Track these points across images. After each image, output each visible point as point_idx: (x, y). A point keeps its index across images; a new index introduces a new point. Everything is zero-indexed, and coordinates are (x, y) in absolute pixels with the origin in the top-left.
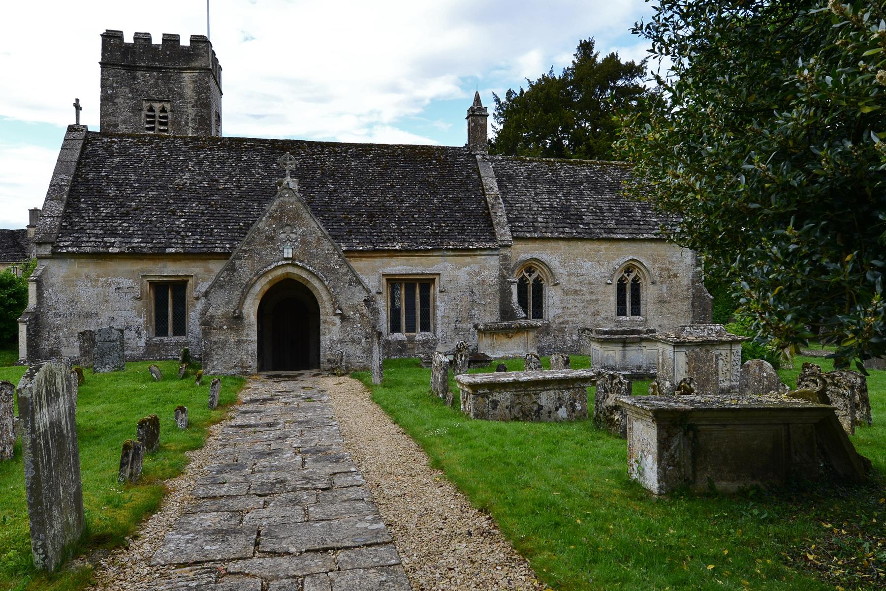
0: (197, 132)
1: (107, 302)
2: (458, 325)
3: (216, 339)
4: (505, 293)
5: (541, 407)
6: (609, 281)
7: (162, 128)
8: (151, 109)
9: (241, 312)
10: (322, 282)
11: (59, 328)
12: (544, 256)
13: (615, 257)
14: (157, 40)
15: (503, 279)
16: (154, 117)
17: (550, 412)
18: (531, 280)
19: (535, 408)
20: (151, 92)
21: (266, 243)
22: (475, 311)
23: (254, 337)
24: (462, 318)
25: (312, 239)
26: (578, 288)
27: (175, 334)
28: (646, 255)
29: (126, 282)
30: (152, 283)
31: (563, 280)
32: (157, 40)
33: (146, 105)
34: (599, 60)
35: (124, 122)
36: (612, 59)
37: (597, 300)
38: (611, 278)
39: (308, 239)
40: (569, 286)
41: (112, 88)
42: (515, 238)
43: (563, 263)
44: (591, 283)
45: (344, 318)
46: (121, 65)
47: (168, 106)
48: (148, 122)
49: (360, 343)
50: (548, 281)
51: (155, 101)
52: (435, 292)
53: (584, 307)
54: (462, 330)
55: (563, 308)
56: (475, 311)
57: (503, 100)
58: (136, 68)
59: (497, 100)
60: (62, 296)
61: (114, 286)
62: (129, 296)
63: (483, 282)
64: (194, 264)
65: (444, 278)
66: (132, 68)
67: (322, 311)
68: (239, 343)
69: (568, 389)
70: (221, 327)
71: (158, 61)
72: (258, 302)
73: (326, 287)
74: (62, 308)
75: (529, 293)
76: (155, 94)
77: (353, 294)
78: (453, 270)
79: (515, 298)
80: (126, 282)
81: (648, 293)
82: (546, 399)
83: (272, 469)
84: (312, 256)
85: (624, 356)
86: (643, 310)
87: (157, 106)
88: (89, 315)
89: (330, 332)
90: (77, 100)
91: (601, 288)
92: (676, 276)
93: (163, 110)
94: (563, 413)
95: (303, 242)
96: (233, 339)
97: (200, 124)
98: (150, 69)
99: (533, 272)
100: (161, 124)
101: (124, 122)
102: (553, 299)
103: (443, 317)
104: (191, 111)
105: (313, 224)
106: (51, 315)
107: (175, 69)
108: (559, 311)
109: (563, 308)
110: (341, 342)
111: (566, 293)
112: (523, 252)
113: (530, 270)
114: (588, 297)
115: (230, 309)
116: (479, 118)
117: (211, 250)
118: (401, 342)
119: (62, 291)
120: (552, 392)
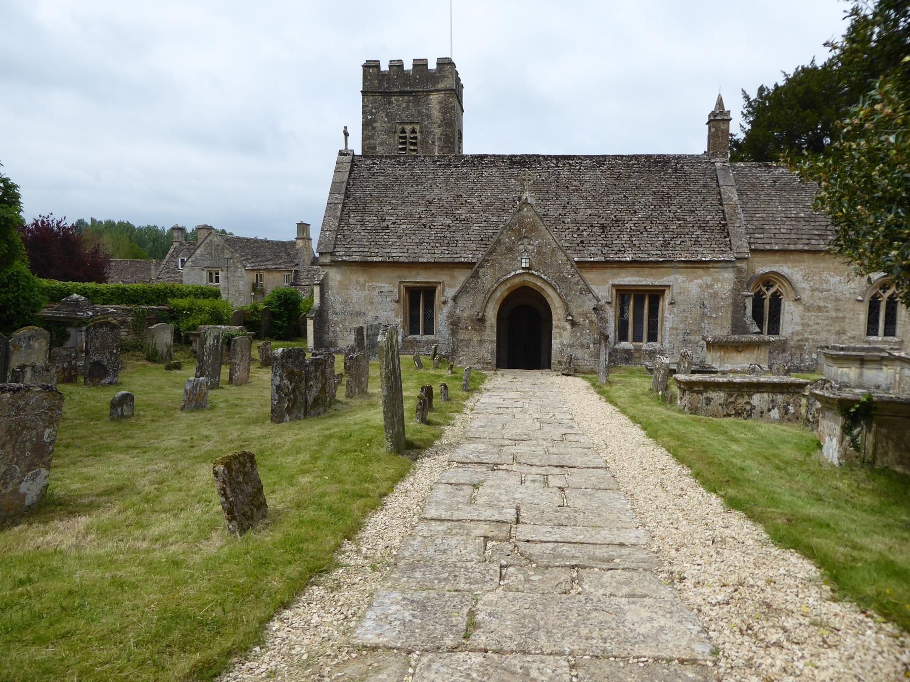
0: (442, 150)
1: (372, 303)
2: (686, 337)
3: (462, 338)
4: (738, 307)
5: (753, 408)
6: (860, 298)
7: (412, 148)
8: (403, 131)
9: (483, 315)
10: (555, 290)
11: (336, 324)
12: (784, 269)
14: (408, 66)
15: (736, 292)
16: (405, 138)
17: (762, 413)
18: (769, 294)
19: (748, 407)
20: (403, 116)
21: (505, 254)
22: (705, 324)
24: (691, 330)
25: (547, 250)
26: (821, 304)
27: (425, 333)
29: (387, 287)
30: (407, 288)
31: (805, 296)
32: (408, 66)
33: (399, 127)
35: (381, 144)
37: (844, 318)
39: (544, 250)
40: (811, 302)
41: (372, 114)
42: (752, 251)
43: (806, 277)
44: (837, 300)
45: (573, 324)
46: (379, 92)
47: (417, 128)
48: (401, 143)
49: (588, 347)
50: (787, 296)
51: (407, 123)
52: (664, 304)
53: (827, 325)
54: (690, 342)
55: (803, 325)
56: (705, 324)
57: (753, 95)
59: (747, 97)
60: (338, 298)
61: (378, 290)
62: (389, 299)
63: (715, 295)
64: (442, 272)
65: (676, 290)
66: (387, 94)
67: (554, 317)
68: (481, 342)
69: (782, 393)
70: (466, 328)
71: (410, 85)
72: (498, 307)
73: (559, 295)
74: (338, 307)
75: (763, 307)
76: (406, 117)
77: (584, 302)
78: (683, 282)
82: (758, 400)
84: (546, 265)
85: (861, 375)
86: (899, 330)
87: (408, 128)
88: (359, 314)
89: (561, 336)
90: (346, 128)
91: (849, 306)
93: (413, 131)
94: (775, 414)
95: (539, 253)
96: (476, 338)
97: (445, 142)
98: (402, 93)
99: (772, 286)
100: (412, 144)
101: (381, 144)
103: (672, 328)
104: (438, 131)
105: (549, 237)
106: (330, 312)
107: (423, 92)
108: (799, 328)
109: (803, 325)
110: (571, 346)
111: (808, 309)
113: (768, 284)
115: (474, 312)
116: (721, 123)
117: (457, 260)
118: (627, 351)
119: (338, 294)
120: (766, 395)
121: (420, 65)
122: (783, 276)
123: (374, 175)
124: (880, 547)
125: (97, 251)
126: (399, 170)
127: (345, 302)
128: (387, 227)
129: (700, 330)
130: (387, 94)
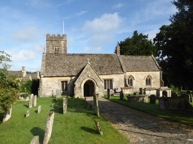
8: (56, 48)
12: (132, 75)
13: (145, 74)
14: (56, 35)
22: (120, 85)
23: (83, 91)
28: (151, 73)
32: (56, 35)
33: (55, 48)
34: (139, 35)
36: (141, 34)
38: (145, 78)
43: (136, 76)
45: (99, 87)
56: (120, 85)
57: (120, 43)
58: (52, 41)
59: (119, 43)
63: (121, 80)
79: (127, 83)
80: (57, 81)
81: (152, 81)
83: (189, 121)
87: (57, 48)
88: (50, 88)
90: (83, 128)
92: (156, 78)
95: (91, 74)
98: (55, 41)
100: (57, 51)
102: (134, 82)
104: (63, 49)
106: (44, 88)
110: (98, 91)
112: (128, 74)
114: (140, 82)
121: (59, 35)
122: (133, 77)
123: (51, 58)
124: (48, 136)
125: (127, 96)
126: (57, 57)
127: (47, 85)
128: (56, 69)
129: (119, 86)
130: (52, 41)
